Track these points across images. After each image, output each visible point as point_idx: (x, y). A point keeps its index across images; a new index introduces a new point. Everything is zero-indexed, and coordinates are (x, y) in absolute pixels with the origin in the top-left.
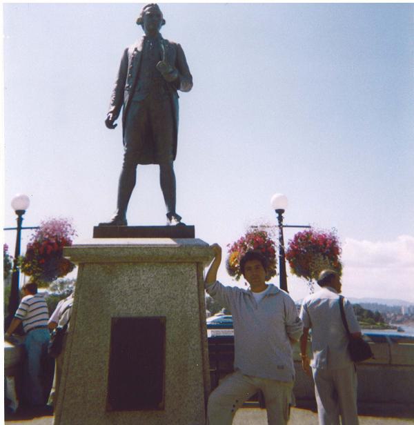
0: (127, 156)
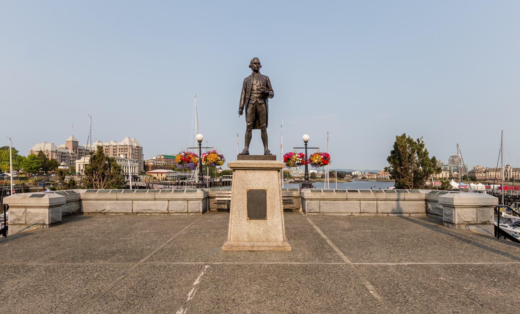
0: (248, 127)
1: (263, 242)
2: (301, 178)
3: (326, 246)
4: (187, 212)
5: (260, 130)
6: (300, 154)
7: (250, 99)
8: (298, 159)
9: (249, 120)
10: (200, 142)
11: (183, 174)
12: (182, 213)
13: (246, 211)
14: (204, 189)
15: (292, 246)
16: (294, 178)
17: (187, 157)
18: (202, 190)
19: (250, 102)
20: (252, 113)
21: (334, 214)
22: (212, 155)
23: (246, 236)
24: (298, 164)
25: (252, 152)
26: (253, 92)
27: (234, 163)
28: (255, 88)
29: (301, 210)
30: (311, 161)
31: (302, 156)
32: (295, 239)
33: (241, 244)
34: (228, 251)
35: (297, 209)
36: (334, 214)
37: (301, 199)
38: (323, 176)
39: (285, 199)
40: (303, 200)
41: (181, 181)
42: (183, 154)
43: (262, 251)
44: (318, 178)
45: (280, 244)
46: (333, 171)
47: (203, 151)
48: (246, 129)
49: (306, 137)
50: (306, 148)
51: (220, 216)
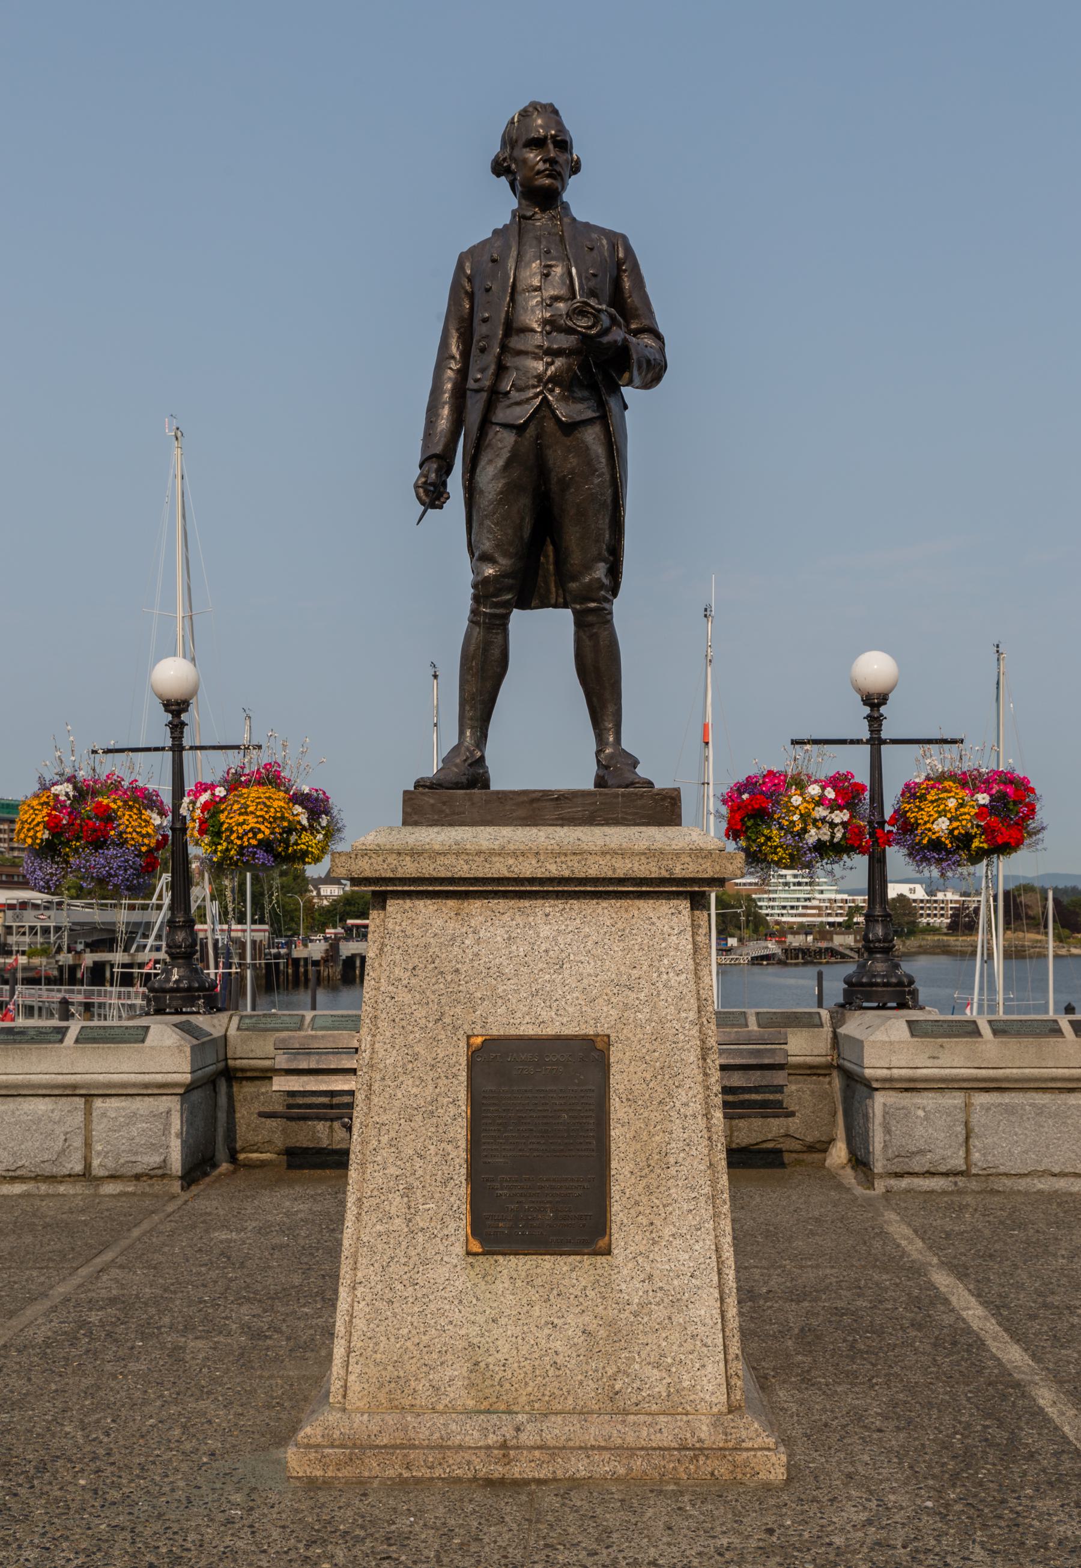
0: (483, 591)
1: (583, 1413)
2: (823, 932)
3: (1029, 1436)
4: (86, 1175)
5: (566, 616)
6: (835, 781)
7: (495, 396)
8: (821, 812)
9: (487, 545)
10: (176, 708)
11: (96, 916)
12: (51, 1179)
13: (464, 1191)
14: (201, 1021)
15: (786, 1441)
16: (782, 932)
17: (87, 808)
18: (187, 1029)
19: (502, 415)
20: (508, 494)
21: (1061, 1184)
22: (254, 792)
23: (459, 1370)
24: (822, 848)
25: (507, 772)
26: (516, 343)
27: (378, 851)
28: (533, 314)
29: (839, 1153)
30: (907, 826)
31: (846, 792)
32: (807, 1381)
33: (424, 1429)
34: (326, 1484)
35: (811, 1148)
36: (1061, 1184)
37: (837, 1082)
38: (963, 922)
39: (737, 1080)
40: (856, 1086)
41: (89, 959)
42: (64, 789)
43: (575, 1483)
44: (930, 929)
45: (705, 1431)
46: (1028, 889)
47: (205, 768)
48: (467, 603)
49: (875, 667)
50: (876, 742)
51: (292, 1202)
